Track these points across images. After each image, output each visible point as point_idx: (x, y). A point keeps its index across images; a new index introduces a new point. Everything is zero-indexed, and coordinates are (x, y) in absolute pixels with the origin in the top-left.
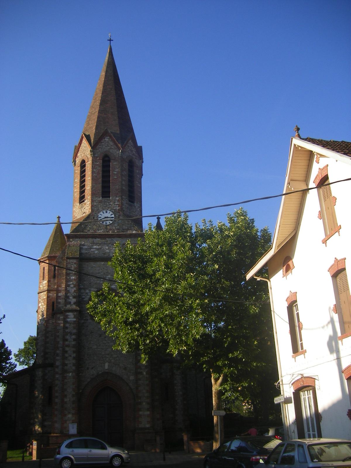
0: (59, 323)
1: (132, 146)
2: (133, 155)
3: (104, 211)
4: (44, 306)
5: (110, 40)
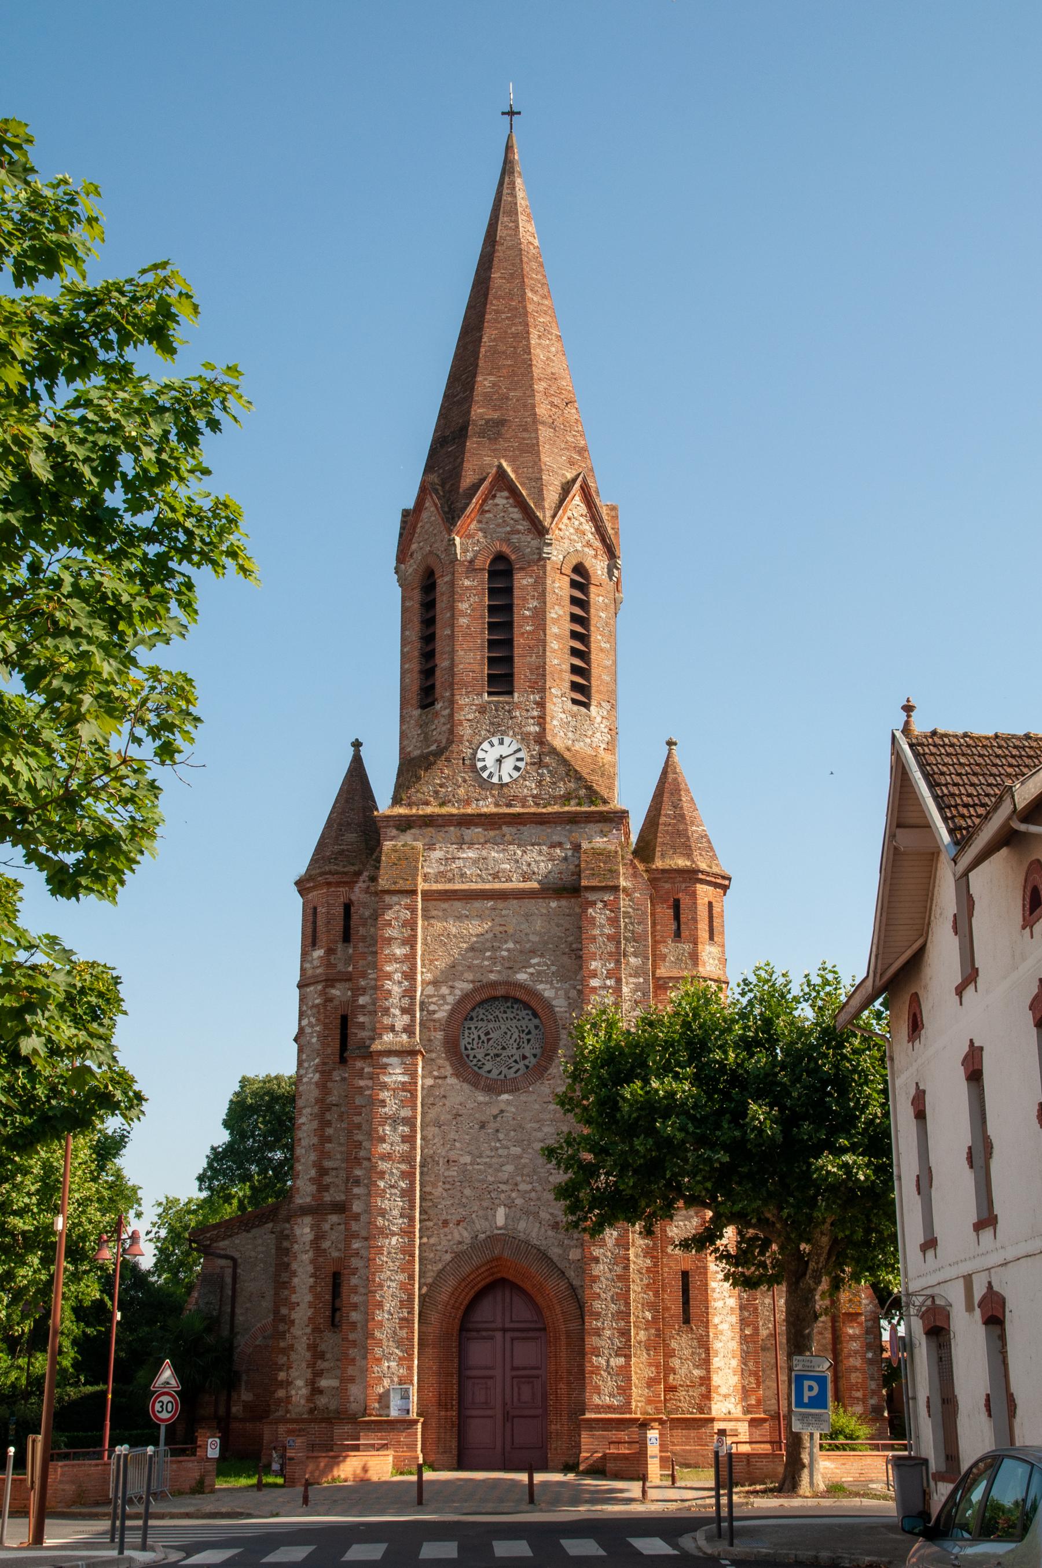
0: (361, 1087)
1: (582, 515)
2: (589, 544)
3: (495, 740)
4: (318, 1029)
5: (511, 113)
